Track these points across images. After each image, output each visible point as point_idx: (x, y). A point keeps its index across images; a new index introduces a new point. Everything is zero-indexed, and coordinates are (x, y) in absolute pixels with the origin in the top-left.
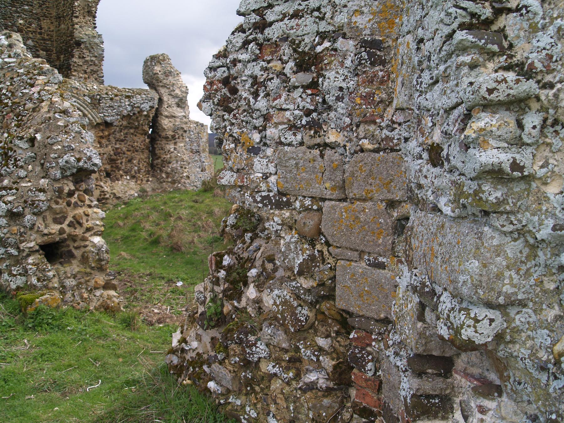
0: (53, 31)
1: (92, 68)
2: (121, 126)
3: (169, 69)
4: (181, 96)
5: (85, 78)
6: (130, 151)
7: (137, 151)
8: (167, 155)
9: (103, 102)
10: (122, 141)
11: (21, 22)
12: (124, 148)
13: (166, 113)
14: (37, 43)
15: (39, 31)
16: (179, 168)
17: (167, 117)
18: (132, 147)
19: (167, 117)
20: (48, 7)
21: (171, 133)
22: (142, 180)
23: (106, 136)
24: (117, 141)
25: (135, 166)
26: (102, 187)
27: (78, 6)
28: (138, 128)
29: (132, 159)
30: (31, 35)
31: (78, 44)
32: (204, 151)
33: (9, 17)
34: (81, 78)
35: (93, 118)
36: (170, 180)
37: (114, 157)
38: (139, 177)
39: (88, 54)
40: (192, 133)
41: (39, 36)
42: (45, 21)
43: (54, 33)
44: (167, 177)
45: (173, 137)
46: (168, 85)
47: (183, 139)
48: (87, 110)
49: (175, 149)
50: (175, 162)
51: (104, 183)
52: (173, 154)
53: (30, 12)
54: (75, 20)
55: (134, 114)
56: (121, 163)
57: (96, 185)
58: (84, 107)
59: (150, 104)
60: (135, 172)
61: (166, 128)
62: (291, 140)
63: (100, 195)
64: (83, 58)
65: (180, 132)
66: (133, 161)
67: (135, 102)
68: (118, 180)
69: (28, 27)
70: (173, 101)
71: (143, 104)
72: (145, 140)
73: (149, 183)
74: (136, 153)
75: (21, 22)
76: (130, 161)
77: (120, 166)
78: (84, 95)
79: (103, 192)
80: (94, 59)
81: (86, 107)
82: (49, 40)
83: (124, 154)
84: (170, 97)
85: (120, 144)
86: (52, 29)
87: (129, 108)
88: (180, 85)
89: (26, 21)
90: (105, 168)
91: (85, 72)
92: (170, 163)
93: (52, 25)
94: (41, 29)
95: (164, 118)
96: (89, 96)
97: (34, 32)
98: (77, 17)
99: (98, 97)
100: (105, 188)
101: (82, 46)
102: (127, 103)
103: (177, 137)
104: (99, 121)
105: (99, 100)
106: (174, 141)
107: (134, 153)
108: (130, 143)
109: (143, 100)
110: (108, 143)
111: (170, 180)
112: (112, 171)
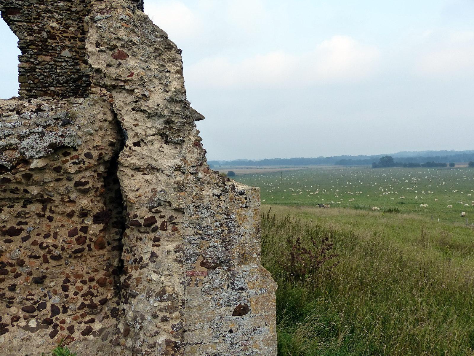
3: (122, 34)
6: (36, 257)
7: (58, 258)
11: (54, 24)
13: (134, 160)
14: (77, 53)
16: (148, 317)
17: (138, 169)
19: (138, 169)
22: (71, 329)
25: (55, 293)
29: (45, 277)
30: (67, 43)
32: (244, 258)
33: (35, 19)
36: (129, 343)
38: (63, 322)
40: (206, 213)
45: (150, 222)
46: (125, 81)
47: (175, 230)
53: (67, 10)
60: (55, 310)
65: (167, 213)
66: (47, 281)
69: (64, 32)
70: (147, 127)
71: (27, 136)
72: (85, 230)
73: (91, 337)
74: (53, 263)
75: (54, 24)
76: (40, 281)
83: (21, 263)
84: (139, 116)
85: (6, 241)
95: (129, 172)
97: (72, 37)
103: (158, 224)
106: (152, 235)
107: (46, 261)
108: (39, 239)
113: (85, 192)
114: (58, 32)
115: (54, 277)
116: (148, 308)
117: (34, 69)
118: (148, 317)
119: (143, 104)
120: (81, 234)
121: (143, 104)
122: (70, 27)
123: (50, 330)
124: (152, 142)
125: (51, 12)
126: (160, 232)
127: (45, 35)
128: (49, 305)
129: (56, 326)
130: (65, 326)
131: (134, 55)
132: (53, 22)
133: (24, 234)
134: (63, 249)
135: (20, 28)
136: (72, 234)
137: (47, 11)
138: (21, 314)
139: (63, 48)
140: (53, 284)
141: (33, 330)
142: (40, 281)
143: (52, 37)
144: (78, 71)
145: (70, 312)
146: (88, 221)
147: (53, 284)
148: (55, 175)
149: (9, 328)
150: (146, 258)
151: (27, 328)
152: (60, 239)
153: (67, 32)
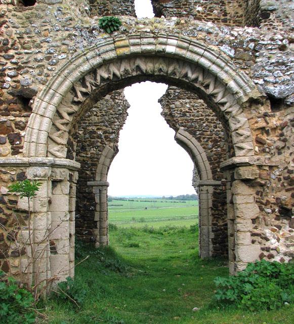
0: (241, 16)
9: (261, 55)
11: (200, 9)
15: (222, 17)
23: (274, 129)
26: (267, 240)
33: (184, 5)
35: (241, 87)
39: (281, 27)
42: (231, 5)
43: (243, 18)
48: (226, 72)
51: (273, 230)
57: (253, 235)
58: (219, 66)
62: (230, 297)
63: (261, 256)
69: (208, 14)
75: (200, 9)
78: (222, 43)
79: (268, 249)
81: (223, 64)
86: (241, 12)
89: (206, 8)
90: (277, 199)
93: (240, 8)
94: (225, 15)
96: (230, 44)
97: (216, 19)
99: (252, 45)
100: (273, 241)
101: (272, 17)
104: (255, 94)
105: (255, 51)
110: (281, 144)
114: (203, 15)
122: (214, 10)
132: (199, 6)
135: (171, 14)
153: (212, 15)
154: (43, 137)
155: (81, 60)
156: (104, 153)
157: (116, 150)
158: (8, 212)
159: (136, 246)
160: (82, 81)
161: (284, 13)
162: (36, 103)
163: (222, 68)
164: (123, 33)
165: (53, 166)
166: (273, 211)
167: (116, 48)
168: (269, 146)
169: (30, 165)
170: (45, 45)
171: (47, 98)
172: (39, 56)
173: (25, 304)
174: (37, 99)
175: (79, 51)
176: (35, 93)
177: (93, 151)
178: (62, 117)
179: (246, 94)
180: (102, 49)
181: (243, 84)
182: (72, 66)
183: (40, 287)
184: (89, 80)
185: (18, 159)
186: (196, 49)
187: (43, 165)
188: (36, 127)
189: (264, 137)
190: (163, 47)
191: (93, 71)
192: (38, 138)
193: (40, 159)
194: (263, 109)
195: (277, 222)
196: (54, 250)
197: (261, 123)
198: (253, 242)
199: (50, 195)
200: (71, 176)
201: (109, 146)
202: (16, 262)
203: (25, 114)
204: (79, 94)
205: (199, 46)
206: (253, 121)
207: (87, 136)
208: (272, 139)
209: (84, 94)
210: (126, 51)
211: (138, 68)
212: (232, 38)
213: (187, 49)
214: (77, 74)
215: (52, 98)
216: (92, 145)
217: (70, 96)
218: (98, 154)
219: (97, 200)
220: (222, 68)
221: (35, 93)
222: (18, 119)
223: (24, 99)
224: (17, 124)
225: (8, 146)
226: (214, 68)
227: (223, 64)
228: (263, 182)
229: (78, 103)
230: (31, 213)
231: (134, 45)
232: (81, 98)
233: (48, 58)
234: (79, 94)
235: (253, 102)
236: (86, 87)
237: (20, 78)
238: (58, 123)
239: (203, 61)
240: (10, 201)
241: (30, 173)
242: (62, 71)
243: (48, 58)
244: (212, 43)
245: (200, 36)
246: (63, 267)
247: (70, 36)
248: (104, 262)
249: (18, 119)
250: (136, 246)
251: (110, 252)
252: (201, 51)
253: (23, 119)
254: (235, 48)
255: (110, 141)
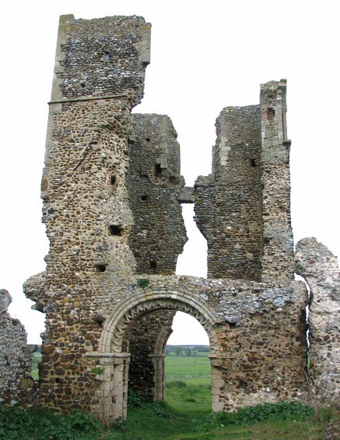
1: (282, 264)
2: (251, 326)
3: (313, 253)
4: (333, 286)
5: (276, 275)
7: (280, 357)
8: (319, 363)
10: (261, 344)
11: (229, 228)
12: (263, 353)
13: (317, 309)
15: (246, 234)
16: (330, 381)
17: (319, 313)
18: (273, 351)
19: (319, 313)
20: (255, 211)
21: (323, 334)
22: (286, 394)
24: (253, 344)
26: (228, 400)
27: (267, 204)
28: (279, 328)
29: (274, 366)
30: (238, 239)
31: (267, 241)
34: (272, 275)
36: (319, 396)
37: (248, 363)
38: (283, 390)
41: (246, 239)
44: (317, 393)
45: (326, 338)
48: (203, 309)
49: (329, 355)
50: (325, 373)
52: (325, 362)
54: (265, 218)
55: (265, 311)
56: (259, 371)
57: (220, 397)
59: (286, 298)
60: (279, 384)
61: (317, 328)
63: (224, 409)
64: (273, 254)
66: (275, 368)
67: (266, 298)
68: (255, 391)
70: (324, 293)
71: (276, 298)
72: (292, 344)
75: (229, 228)
76: (271, 369)
77: (258, 374)
78: (202, 292)
79: (227, 405)
80: (283, 254)
81: (201, 305)
82: (257, 241)
83: (263, 359)
84: (320, 288)
85: (258, 348)
87: (257, 305)
88: (331, 272)
90: (237, 377)
91: (277, 270)
92: (320, 374)
95: (316, 315)
97: (242, 236)
98: (267, 215)
101: (271, 242)
102: (254, 299)
103: (331, 339)
106: (328, 345)
107: (275, 358)
108: (272, 348)
109: (276, 294)
111: (319, 396)
112: (249, 380)
113: (294, 324)
115: (278, 367)
116: (329, 377)
117: (217, 259)
118: (330, 381)
119: (322, 283)
120: (291, 346)
121: (322, 283)
123: (277, 393)
124: (326, 300)
125: (227, 220)
126: (331, 343)
127: (224, 235)
128: (275, 380)
129: (279, 391)
130: (284, 392)
131: (318, 261)
133: (265, 345)
134: (283, 352)
136: (287, 345)
137: (224, 220)
138: (263, 385)
139: (236, 243)
140: (277, 370)
141: (268, 393)
142: (271, 369)
143: (228, 236)
144: (245, 258)
145: (285, 385)
146: (294, 340)
147: (277, 370)
148: (283, 316)
149: (258, 391)
150: (325, 356)
151: (266, 391)
152: (282, 347)
154: (109, 342)
155: (127, 302)
156: (161, 334)
157: (171, 331)
158: (91, 381)
159: (193, 401)
160: (129, 312)
161: (279, 239)
162: (105, 324)
163: (201, 307)
164: (150, 288)
165: (114, 357)
166: (234, 384)
167: (146, 296)
168: (229, 348)
169: (102, 357)
170: (110, 294)
171: (111, 322)
172: (107, 300)
173: (97, 426)
174: (106, 323)
175: (127, 298)
176: (105, 319)
177: (153, 332)
178: (119, 331)
179: (213, 321)
180: (139, 296)
181: (212, 315)
182: (123, 306)
183: (106, 420)
184: (133, 311)
185: (96, 354)
186: (187, 296)
187: (108, 357)
188: (105, 337)
189: (226, 343)
190: (170, 295)
191: (135, 307)
192: (106, 343)
193: (107, 354)
194: (224, 328)
195: (237, 390)
196: (114, 401)
197: (224, 336)
198: (220, 401)
199: (112, 372)
200: (124, 361)
201: (164, 330)
202: (94, 407)
203: (100, 329)
204: (128, 319)
205: (189, 295)
206: (219, 334)
207: (149, 322)
208: (232, 344)
209: (130, 319)
210: (151, 297)
211: (158, 305)
212: (210, 288)
213: (183, 296)
214: (126, 310)
215: (113, 322)
216: (152, 328)
217: (123, 320)
218: (156, 335)
219: (155, 367)
220: (201, 307)
221: (105, 319)
222: (96, 333)
223: (99, 322)
224: (96, 335)
225: (91, 347)
226: (197, 307)
227: (201, 305)
228: (226, 368)
229: (127, 324)
230: (102, 382)
231: (155, 294)
232: (128, 321)
233: (111, 301)
234: (128, 319)
235: (218, 325)
236: (131, 315)
237: (97, 311)
238: (117, 334)
239: (191, 303)
240: (92, 375)
241: (102, 361)
242: (118, 308)
243: (111, 301)
244: (196, 292)
245: (190, 289)
246: (120, 409)
247: (122, 289)
248: (156, 411)
249: (96, 333)
250: (193, 401)
251: (163, 404)
252: (190, 297)
253: (99, 333)
254: (209, 296)
255: (165, 325)
